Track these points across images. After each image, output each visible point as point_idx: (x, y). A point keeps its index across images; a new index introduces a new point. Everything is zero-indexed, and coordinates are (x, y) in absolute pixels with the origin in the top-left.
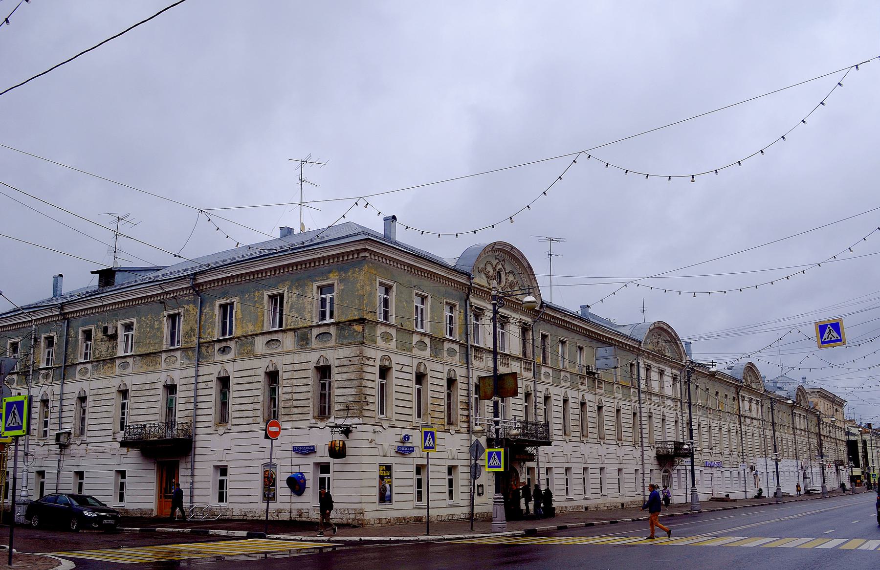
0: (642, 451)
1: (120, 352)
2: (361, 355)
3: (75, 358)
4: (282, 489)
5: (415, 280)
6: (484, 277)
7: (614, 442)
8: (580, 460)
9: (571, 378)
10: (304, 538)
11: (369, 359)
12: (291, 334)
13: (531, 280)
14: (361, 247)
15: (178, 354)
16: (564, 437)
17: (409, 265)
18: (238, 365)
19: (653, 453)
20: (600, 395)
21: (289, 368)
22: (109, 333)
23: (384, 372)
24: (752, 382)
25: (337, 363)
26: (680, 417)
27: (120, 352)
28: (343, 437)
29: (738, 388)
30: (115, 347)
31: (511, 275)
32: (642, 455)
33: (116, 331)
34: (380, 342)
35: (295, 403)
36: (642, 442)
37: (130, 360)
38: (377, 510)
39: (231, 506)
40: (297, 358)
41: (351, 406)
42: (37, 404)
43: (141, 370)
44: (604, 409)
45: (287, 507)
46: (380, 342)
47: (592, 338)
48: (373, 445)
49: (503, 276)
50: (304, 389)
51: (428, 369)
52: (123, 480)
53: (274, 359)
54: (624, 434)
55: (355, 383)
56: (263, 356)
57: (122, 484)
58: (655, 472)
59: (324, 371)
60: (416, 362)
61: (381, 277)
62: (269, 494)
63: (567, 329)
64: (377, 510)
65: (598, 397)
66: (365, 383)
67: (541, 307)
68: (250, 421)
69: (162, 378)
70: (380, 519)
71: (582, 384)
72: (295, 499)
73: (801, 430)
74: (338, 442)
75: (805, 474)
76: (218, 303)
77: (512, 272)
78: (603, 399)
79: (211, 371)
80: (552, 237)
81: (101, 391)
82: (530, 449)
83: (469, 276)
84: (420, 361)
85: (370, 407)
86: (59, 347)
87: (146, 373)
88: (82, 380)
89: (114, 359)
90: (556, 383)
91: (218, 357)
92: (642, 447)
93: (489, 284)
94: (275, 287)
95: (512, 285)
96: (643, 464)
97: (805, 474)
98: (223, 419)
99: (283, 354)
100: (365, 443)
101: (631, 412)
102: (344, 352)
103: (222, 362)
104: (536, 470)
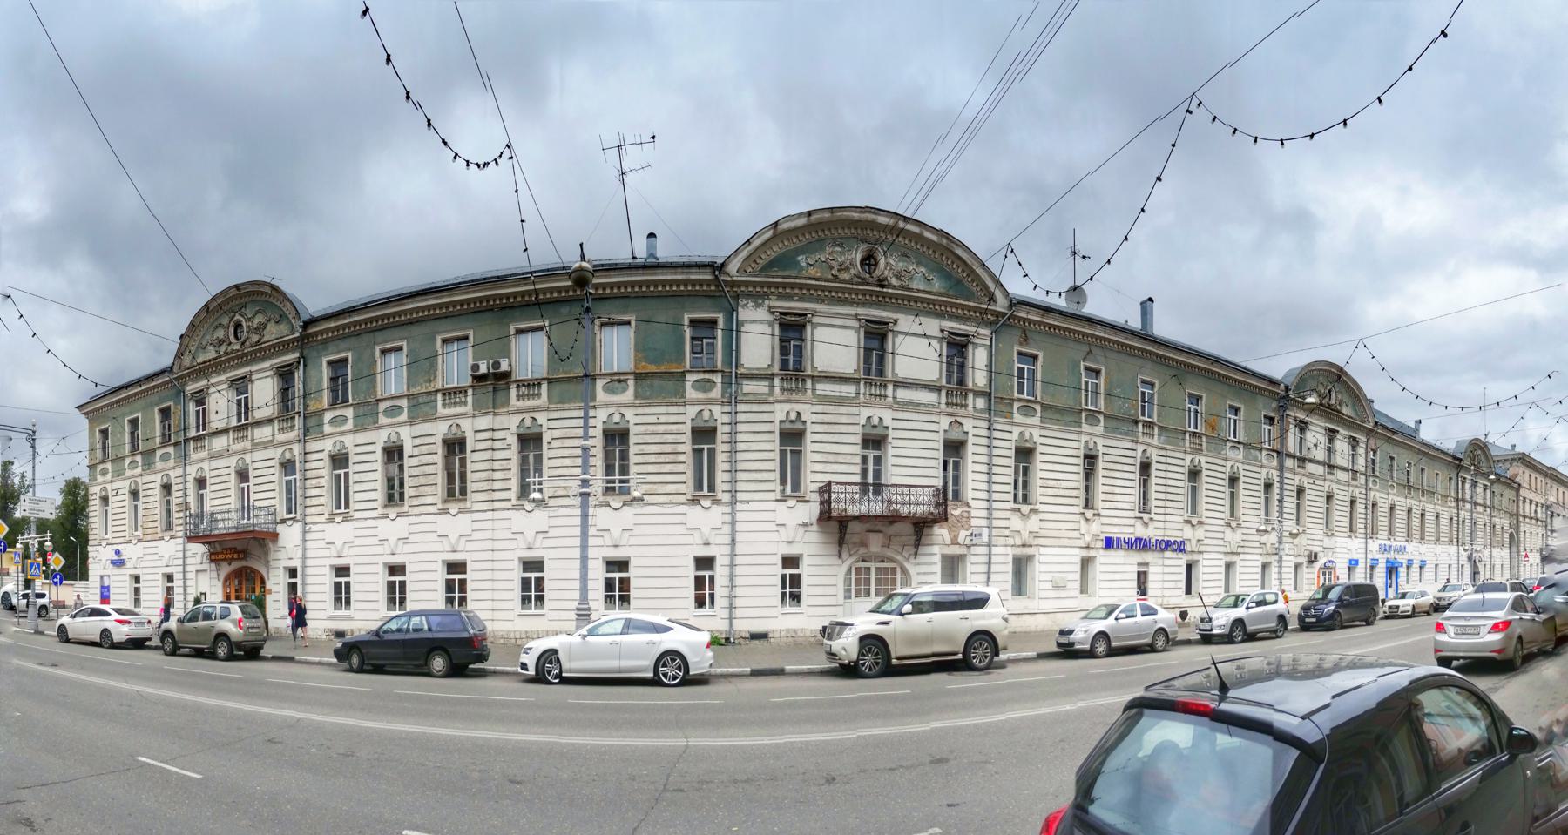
57: (136, 589)
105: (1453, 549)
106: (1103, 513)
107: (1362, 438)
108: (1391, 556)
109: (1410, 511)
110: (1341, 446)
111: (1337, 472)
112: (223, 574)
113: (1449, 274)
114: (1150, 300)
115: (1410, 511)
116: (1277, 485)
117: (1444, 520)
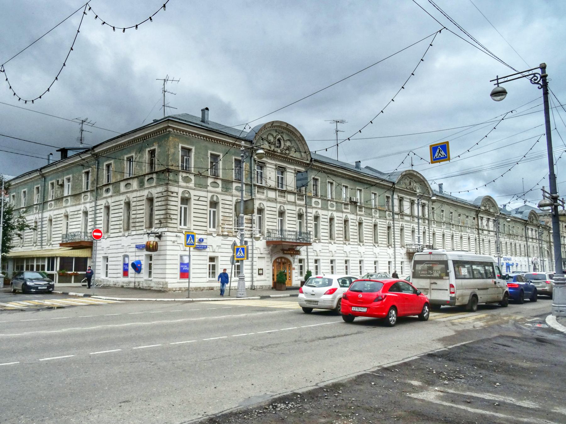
0: (395, 250)
1: (66, 194)
2: (167, 191)
3: (47, 199)
4: (131, 270)
5: (209, 145)
6: (266, 143)
7: (372, 244)
8: (343, 255)
9: (337, 206)
10: (108, 298)
11: (172, 193)
12: (136, 180)
13: (303, 145)
14: (166, 125)
15: (89, 194)
16: (330, 241)
17: (204, 136)
18: (114, 199)
19: (404, 251)
20: (360, 215)
21: (135, 199)
22: (60, 183)
23: (185, 201)
24: (490, 208)
25: (156, 195)
26: (427, 230)
27: (66, 194)
28: (157, 239)
29: (478, 212)
30: (63, 191)
31: (289, 142)
32: (395, 253)
33: (63, 182)
34: (182, 183)
35: (137, 220)
36: (394, 244)
37: (69, 198)
38: (178, 282)
39: (109, 279)
40: (139, 194)
41: (163, 221)
42: (46, 222)
43: (74, 204)
44: (364, 224)
45: (133, 280)
46: (182, 183)
47: (355, 181)
48: (176, 244)
49: (282, 142)
50: (141, 211)
51: (220, 199)
52: (151, 262)
53: (128, 195)
54: (379, 239)
55: (164, 207)
56: (124, 193)
57: (150, 264)
58: (405, 263)
59: (150, 200)
60: (210, 195)
61: (182, 143)
62: (126, 273)
63: (335, 175)
64: (178, 282)
65: (358, 217)
66: (169, 207)
67: (311, 161)
68: (118, 231)
69: (82, 207)
70: (180, 288)
71: (345, 208)
72: (137, 275)
73: (532, 238)
74: (152, 243)
75: (535, 266)
76: (105, 164)
77: (289, 140)
78: (363, 218)
79: (102, 203)
80: (338, 119)
81: (58, 216)
82: (298, 248)
83: (251, 142)
84: (213, 194)
85: (174, 221)
86: (41, 194)
87: (76, 205)
88: (50, 210)
89: (62, 198)
90: (324, 208)
91: (105, 195)
92: (395, 247)
93: (270, 147)
94: (130, 153)
95: (288, 149)
96: (395, 258)
97: (535, 266)
98: (331, 237)
99: (132, 191)
100: (171, 243)
101: (386, 226)
102: (160, 189)
103: (106, 198)
104: (306, 261)
105: (526, 259)
106: (380, 245)
107: (416, 199)
108: (507, 261)
109: (511, 243)
110: (406, 205)
111: (491, 233)
112: (273, 259)
113: (448, 96)
114: (207, 109)
115: (511, 243)
116: (392, 227)
117: (522, 247)
